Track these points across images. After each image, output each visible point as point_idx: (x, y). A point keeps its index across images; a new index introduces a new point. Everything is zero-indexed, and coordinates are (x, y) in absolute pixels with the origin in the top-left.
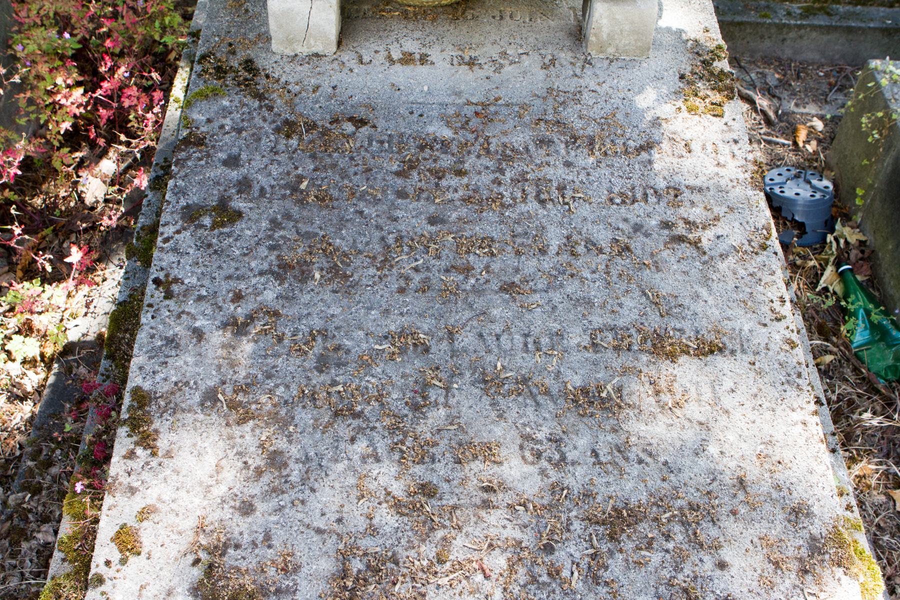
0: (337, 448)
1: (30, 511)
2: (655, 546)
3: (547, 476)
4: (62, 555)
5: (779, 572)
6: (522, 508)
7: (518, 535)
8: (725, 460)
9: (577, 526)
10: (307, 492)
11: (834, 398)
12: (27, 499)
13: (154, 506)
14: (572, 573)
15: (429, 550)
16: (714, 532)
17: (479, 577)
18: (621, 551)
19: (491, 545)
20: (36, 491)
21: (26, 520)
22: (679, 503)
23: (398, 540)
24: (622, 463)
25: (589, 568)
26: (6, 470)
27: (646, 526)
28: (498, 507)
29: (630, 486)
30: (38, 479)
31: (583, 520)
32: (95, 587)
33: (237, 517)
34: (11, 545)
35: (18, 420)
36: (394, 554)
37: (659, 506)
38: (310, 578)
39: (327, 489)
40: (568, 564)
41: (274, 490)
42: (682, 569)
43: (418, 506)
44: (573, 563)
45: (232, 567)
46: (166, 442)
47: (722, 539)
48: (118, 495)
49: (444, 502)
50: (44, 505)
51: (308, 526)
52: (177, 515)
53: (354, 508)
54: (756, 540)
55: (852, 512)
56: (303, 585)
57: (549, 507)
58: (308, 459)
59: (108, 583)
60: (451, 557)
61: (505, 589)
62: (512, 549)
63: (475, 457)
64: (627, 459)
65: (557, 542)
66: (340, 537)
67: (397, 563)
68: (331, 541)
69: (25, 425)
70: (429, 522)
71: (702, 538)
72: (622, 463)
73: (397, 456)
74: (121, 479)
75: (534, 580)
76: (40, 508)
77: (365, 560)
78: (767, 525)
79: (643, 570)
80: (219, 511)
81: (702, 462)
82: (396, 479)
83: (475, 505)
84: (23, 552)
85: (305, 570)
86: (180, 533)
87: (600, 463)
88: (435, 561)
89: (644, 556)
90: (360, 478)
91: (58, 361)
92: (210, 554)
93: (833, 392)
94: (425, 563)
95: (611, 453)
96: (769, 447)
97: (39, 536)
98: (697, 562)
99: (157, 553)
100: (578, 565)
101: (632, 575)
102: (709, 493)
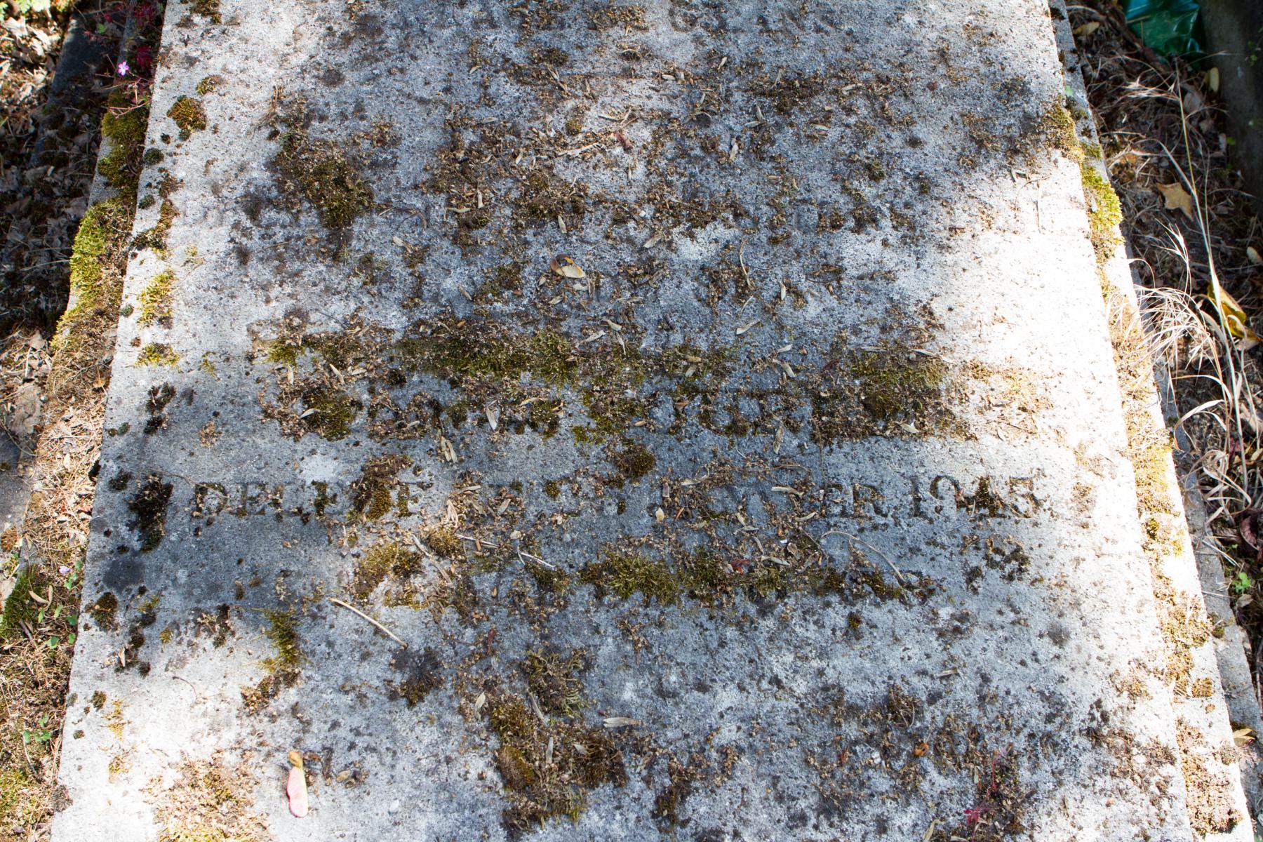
0: (443, 13)
1: (55, 184)
2: (833, 119)
3: (703, 44)
4: (104, 179)
5: (983, 152)
6: (671, 77)
7: (666, 105)
8: (924, 30)
9: (737, 97)
10: (407, 60)
11: (1096, 74)
12: (49, 172)
13: (218, 77)
14: (731, 147)
15: (556, 122)
16: (906, 107)
17: (618, 150)
18: (791, 125)
19: (632, 116)
20: (61, 162)
21: (51, 195)
22: (865, 75)
23: (520, 110)
24: (797, 32)
25: (752, 141)
26: (19, 148)
27: (823, 99)
28: (641, 77)
29: (804, 55)
30: (61, 149)
31: (746, 91)
32: (152, 163)
33: (321, 88)
34: (33, 222)
35: (28, 91)
36: (514, 125)
37: (839, 78)
38: (411, 151)
39: (431, 56)
40: (726, 137)
41: (366, 58)
42: (865, 145)
43: (543, 73)
44: (732, 136)
45: (316, 139)
46: (229, 7)
47: (915, 115)
48: (173, 66)
49: (576, 70)
50: (72, 178)
51: (409, 96)
52: (248, 86)
53: (465, 77)
54: (956, 117)
55: (1090, 137)
56: (404, 157)
57: (705, 78)
58: (407, 24)
59: (168, 160)
60: (584, 129)
61: (649, 163)
62: (658, 121)
63: (614, 23)
64: (802, 28)
65: (713, 113)
66: (448, 107)
67: (518, 136)
68: (437, 112)
69: (39, 99)
70: (557, 91)
71: (891, 112)
72: (797, 32)
73: (517, 21)
74: (176, 49)
75: (684, 153)
76: (67, 182)
77: (479, 131)
78: (972, 102)
79: (818, 145)
80: (299, 81)
81: (895, 32)
82: (516, 45)
83: (614, 74)
84: (49, 230)
85: (406, 142)
86: (252, 105)
87: (769, 31)
88: (564, 132)
89: (819, 131)
90: (472, 44)
91: (76, 15)
92: (289, 126)
93: (1095, 67)
94: (552, 134)
95: (782, 20)
96: (980, 18)
97: (69, 211)
98: (884, 138)
99: (225, 127)
100: (738, 139)
101: (804, 150)
102: (901, 65)
